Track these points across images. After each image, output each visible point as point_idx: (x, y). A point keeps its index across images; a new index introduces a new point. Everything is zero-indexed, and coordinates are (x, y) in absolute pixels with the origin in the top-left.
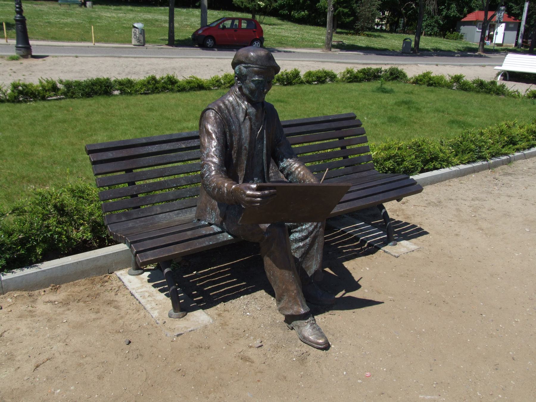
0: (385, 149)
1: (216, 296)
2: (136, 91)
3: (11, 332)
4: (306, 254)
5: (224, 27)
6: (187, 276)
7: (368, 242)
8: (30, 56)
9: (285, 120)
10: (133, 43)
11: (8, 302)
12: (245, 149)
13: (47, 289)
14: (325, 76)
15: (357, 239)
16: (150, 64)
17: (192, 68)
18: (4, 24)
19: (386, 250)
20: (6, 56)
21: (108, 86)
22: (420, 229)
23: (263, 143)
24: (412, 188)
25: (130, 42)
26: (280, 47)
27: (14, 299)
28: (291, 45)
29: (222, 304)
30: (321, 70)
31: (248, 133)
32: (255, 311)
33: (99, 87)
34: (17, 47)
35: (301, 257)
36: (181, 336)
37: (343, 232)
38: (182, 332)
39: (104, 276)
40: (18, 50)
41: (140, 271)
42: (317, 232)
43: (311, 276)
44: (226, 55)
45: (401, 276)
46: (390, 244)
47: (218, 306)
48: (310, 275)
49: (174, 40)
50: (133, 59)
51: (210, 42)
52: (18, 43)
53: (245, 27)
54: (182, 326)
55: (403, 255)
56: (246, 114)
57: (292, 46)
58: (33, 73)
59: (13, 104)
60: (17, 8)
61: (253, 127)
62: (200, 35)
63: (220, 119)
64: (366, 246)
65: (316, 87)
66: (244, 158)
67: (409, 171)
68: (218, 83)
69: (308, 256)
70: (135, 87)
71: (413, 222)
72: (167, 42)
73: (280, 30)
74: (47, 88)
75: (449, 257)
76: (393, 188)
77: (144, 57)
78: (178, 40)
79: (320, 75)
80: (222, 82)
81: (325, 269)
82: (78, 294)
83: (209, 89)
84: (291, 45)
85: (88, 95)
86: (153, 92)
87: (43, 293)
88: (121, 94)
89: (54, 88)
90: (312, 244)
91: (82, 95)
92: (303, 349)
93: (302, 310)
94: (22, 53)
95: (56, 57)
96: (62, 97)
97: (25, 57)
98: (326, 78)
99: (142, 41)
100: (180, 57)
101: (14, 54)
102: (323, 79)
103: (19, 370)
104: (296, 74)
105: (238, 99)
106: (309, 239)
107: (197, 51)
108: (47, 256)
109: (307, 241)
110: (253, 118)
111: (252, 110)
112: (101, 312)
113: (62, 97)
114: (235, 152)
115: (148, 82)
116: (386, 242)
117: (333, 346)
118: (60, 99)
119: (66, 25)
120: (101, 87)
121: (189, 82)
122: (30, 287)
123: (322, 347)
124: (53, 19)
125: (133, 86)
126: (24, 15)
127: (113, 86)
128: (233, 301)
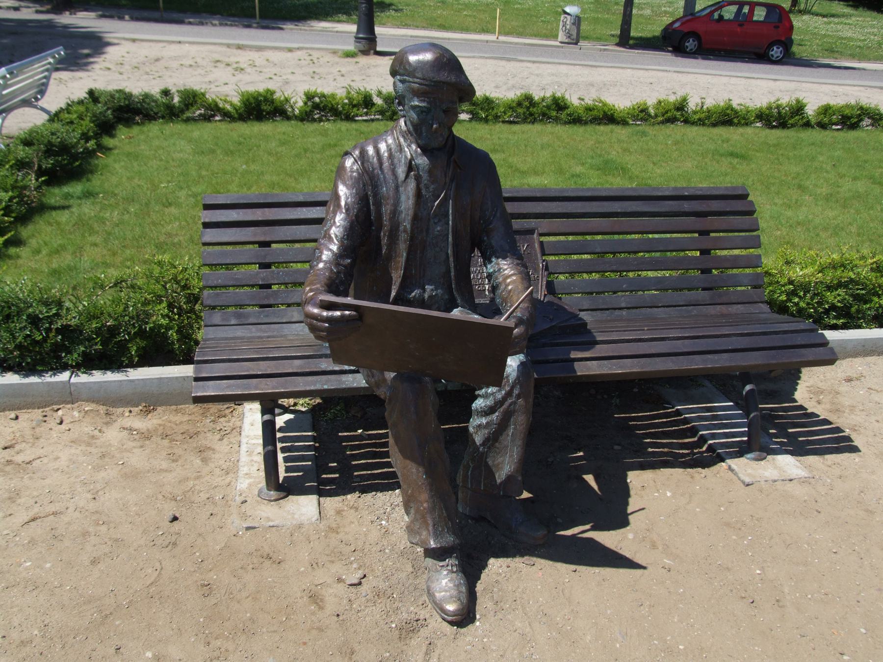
0: (834, 266)
1: (358, 479)
2: (496, 117)
3: (45, 460)
4: (494, 438)
5: (721, 17)
6: (345, 434)
7: (711, 442)
8: (372, 52)
10: (560, 39)
11: (73, 416)
12: (405, 231)
13: (136, 410)
14: (860, 115)
15: (693, 431)
16: (553, 75)
17: (622, 86)
19: (734, 466)
20: (339, 50)
22: (848, 439)
23: (448, 224)
24: (819, 352)
25: (555, 37)
26: (827, 57)
27: (83, 414)
28: (850, 55)
29: (357, 494)
30: (853, 102)
31: (411, 202)
32: (381, 522)
34: (356, 38)
35: (484, 444)
37: (678, 413)
38: (256, 525)
39: (226, 406)
42: (510, 405)
43: (501, 483)
44: (706, 68)
45: (728, 524)
46: (749, 456)
47: (349, 496)
48: (499, 481)
49: (629, 37)
50: (529, 65)
51: (691, 44)
52: (358, 32)
53: (762, 19)
54: (264, 515)
55: (763, 483)
56: (410, 167)
57: (853, 57)
58: (368, 79)
59: (300, 123)
61: (424, 192)
62: (674, 30)
63: (359, 174)
64: (704, 449)
65: (837, 136)
66: (402, 248)
67: (819, 321)
68: (642, 115)
69: (497, 444)
70: (495, 111)
71: (837, 421)
72: (617, 40)
73: (839, 27)
74: (355, 102)
75: (867, 511)
76: (762, 346)
77: (548, 63)
78: (640, 39)
79: (847, 112)
80: (652, 111)
81: (585, 477)
82: (174, 426)
83: (624, 123)
84: (850, 55)
86: (525, 121)
87: (127, 414)
88: (471, 120)
90: (503, 425)
92: (423, 612)
93: (432, 543)
94: (362, 48)
97: (365, 53)
98: (862, 120)
99: (575, 36)
100: (610, 65)
101: (351, 47)
102: (854, 120)
103: (8, 519)
104: (798, 109)
105: (402, 140)
106: (497, 414)
107: (666, 58)
108: (147, 359)
109: (495, 417)
110: (425, 176)
111: (422, 161)
112: (179, 463)
114: (385, 234)
115: (519, 104)
116: (741, 451)
117: (478, 623)
118: (373, 120)
121: (589, 109)
122: (112, 400)
123: (450, 618)
125: (493, 109)
128: (379, 494)
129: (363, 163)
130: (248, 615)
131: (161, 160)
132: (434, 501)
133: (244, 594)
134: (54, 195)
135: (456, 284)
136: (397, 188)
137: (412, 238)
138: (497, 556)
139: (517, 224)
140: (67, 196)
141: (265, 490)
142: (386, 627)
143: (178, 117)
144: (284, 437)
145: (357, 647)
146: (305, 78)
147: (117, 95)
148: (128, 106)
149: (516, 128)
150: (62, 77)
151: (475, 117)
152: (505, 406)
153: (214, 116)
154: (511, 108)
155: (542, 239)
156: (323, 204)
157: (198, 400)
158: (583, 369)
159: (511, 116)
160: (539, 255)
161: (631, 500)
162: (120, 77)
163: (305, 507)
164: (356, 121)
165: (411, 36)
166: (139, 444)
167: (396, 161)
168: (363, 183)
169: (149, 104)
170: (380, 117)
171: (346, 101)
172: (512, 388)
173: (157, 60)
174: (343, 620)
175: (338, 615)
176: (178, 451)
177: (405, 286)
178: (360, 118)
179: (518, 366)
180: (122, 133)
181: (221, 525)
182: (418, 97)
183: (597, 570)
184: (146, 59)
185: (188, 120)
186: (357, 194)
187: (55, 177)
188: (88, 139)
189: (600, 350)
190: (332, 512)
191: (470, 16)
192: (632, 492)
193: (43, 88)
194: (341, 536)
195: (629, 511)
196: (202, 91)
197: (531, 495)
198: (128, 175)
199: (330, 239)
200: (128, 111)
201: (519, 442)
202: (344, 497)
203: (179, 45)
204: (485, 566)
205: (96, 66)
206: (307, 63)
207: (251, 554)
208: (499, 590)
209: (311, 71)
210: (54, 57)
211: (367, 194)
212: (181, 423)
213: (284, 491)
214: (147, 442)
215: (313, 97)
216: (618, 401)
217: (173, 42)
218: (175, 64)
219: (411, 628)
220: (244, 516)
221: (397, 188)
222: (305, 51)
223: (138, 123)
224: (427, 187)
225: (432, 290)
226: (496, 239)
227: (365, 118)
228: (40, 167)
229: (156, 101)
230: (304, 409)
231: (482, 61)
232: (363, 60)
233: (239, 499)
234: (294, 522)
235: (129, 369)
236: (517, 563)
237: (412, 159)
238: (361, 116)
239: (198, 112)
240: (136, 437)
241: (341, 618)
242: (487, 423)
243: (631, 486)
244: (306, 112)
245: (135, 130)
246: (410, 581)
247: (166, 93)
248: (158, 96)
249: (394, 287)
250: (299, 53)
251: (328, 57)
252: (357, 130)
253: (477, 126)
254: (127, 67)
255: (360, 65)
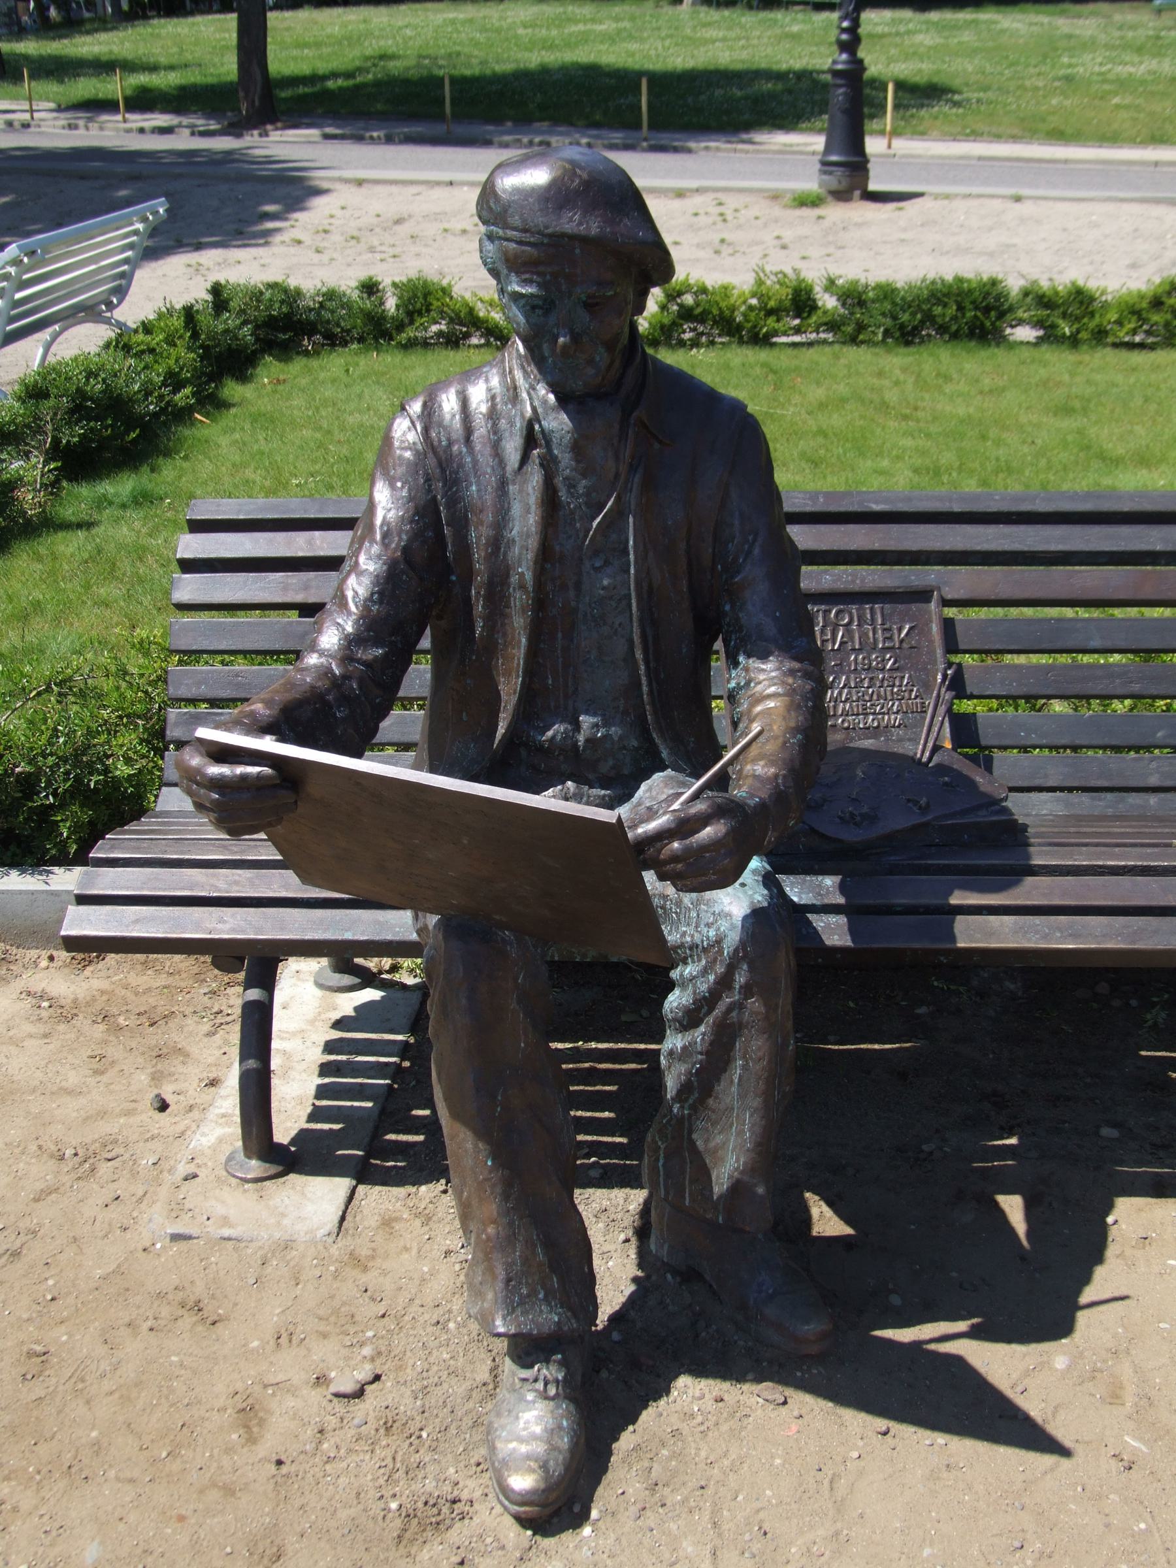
8: (857, 193)
9: (1065, 487)
12: (522, 586)
18: (891, 87)
20: (786, 191)
21: (987, 310)
33: (952, 310)
34: (824, 163)
36: (183, 1245)
38: (194, 1231)
40: (825, 173)
41: (348, 980)
42: (730, 1009)
43: (720, 1197)
47: (423, 1188)
52: (828, 150)
54: (220, 1210)
56: (531, 439)
60: (844, 30)
61: (563, 494)
63: (417, 453)
66: (519, 623)
69: (711, 1101)
70: (1097, 320)
74: (772, 304)
81: (1001, 1199)
85: (906, 335)
87: (44, 963)
88: (1040, 341)
89: (801, 302)
91: (887, 333)
92: (471, 1483)
95: (947, 197)
96: (822, 336)
97: (841, 196)
106: (702, 1029)
110: (565, 458)
111: (558, 423)
112: (105, 1079)
113: (822, 336)
114: (478, 593)
115: (1157, 303)
117: (587, 1531)
118: (810, 344)
119: (1123, 84)
120: (960, 308)
124: (1088, 65)
126: (861, 54)
127: (1011, 309)
129: (426, 430)
130: (94, 1434)
131: (319, 428)
132: (511, 1224)
133: (107, 1385)
134: (77, 497)
135: (655, 713)
136: (503, 484)
137: (540, 602)
138: (700, 1372)
139: (814, 578)
140: (102, 502)
141: (241, 1156)
142: (376, 1508)
143: (391, 339)
144: (341, 1040)
145: (292, 1543)
146: (701, 254)
147: (268, 295)
148: (288, 316)
149: (1137, 358)
150: (202, 261)
151: (1050, 336)
152: (717, 1012)
153: (467, 336)
154: (1136, 312)
155: (951, 612)
156: (346, 524)
157: (75, 944)
158: (970, 934)
159: (1134, 332)
160: (939, 652)
161: (1100, 1273)
162: (316, 258)
163: (318, 1198)
164: (773, 345)
165: (980, 158)
166: (41, 1028)
167: (503, 423)
168: (426, 474)
169: (333, 312)
170: (830, 337)
171: (754, 302)
172: (731, 969)
173: (399, 222)
174: (287, 1476)
175: (279, 1463)
176: (114, 1051)
177: (532, 708)
178: (784, 339)
179: (745, 918)
180: (269, 370)
181: (126, 1223)
182: (518, 273)
183: (941, 1439)
184: (375, 221)
185: (410, 345)
186: (410, 499)
187: (77, 464)
188: (178, 386)
189: (1032, 890)
190: (373, 1221)
191: (1127, 107)
192: (1111, 1252)
193: (123, 282)
194: (370, 1278)
195: (1084, 1299)
196: (445, 283)
197: (849, 1231)
198: (237, 458)
199: (342, 603)
200: (289, 328)
201: (756, 1102)
202: (412, 1189)
203: (449, 189)
204: (663, 1390)
205: (277, 238)
206: (710, 220)
207: (161, 1296)
208: (674, 1455)
209: (717, 237)
210: (144, 220)
211: (435, 498)
212: (149, 990)
213: (278, 1163)
214: (62, 1027)
215: (680, 294)
216: (1163, 1015)
217: (438, 183)
218: (431, 229)
219: (435, 1515)
220: (177, 1209)
221: (503, 484)
222: (712, 195)
223: (306, 353)
224: (571, 485)
225: (596, 725)
226: (756, 607)
227: (797, 339)
228: (56, 441)
229: (348, 305)
230: (410, 981)
231: (1110, 207)
232: (836, 212)
233: (183, 1169)
234: (277, 1235)
235: (56, 869)
236: (752, 1397)
237: (536, 418)
238: (785, 334)
239: (435, 328)
240: (45, 1014)
241: (284, 1469)
242: (684, 1048)
243: (1113, 1232)
244: (662, 327)
245: (297, 365)
246: (471, 1405)
247: (370, 288)
248: (355, 295)
249: (502, 715)
250: (697, 201)
251: (761, 208)
252: (765, 365)
253: (1048, 356)
254: (336, 238)
255: (826, 223)
